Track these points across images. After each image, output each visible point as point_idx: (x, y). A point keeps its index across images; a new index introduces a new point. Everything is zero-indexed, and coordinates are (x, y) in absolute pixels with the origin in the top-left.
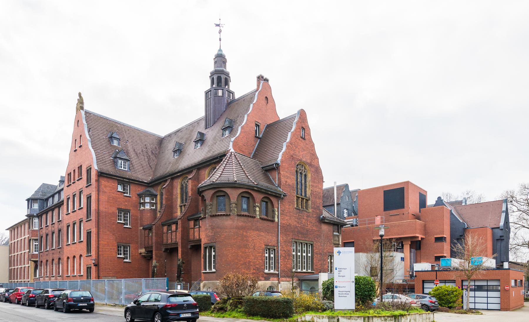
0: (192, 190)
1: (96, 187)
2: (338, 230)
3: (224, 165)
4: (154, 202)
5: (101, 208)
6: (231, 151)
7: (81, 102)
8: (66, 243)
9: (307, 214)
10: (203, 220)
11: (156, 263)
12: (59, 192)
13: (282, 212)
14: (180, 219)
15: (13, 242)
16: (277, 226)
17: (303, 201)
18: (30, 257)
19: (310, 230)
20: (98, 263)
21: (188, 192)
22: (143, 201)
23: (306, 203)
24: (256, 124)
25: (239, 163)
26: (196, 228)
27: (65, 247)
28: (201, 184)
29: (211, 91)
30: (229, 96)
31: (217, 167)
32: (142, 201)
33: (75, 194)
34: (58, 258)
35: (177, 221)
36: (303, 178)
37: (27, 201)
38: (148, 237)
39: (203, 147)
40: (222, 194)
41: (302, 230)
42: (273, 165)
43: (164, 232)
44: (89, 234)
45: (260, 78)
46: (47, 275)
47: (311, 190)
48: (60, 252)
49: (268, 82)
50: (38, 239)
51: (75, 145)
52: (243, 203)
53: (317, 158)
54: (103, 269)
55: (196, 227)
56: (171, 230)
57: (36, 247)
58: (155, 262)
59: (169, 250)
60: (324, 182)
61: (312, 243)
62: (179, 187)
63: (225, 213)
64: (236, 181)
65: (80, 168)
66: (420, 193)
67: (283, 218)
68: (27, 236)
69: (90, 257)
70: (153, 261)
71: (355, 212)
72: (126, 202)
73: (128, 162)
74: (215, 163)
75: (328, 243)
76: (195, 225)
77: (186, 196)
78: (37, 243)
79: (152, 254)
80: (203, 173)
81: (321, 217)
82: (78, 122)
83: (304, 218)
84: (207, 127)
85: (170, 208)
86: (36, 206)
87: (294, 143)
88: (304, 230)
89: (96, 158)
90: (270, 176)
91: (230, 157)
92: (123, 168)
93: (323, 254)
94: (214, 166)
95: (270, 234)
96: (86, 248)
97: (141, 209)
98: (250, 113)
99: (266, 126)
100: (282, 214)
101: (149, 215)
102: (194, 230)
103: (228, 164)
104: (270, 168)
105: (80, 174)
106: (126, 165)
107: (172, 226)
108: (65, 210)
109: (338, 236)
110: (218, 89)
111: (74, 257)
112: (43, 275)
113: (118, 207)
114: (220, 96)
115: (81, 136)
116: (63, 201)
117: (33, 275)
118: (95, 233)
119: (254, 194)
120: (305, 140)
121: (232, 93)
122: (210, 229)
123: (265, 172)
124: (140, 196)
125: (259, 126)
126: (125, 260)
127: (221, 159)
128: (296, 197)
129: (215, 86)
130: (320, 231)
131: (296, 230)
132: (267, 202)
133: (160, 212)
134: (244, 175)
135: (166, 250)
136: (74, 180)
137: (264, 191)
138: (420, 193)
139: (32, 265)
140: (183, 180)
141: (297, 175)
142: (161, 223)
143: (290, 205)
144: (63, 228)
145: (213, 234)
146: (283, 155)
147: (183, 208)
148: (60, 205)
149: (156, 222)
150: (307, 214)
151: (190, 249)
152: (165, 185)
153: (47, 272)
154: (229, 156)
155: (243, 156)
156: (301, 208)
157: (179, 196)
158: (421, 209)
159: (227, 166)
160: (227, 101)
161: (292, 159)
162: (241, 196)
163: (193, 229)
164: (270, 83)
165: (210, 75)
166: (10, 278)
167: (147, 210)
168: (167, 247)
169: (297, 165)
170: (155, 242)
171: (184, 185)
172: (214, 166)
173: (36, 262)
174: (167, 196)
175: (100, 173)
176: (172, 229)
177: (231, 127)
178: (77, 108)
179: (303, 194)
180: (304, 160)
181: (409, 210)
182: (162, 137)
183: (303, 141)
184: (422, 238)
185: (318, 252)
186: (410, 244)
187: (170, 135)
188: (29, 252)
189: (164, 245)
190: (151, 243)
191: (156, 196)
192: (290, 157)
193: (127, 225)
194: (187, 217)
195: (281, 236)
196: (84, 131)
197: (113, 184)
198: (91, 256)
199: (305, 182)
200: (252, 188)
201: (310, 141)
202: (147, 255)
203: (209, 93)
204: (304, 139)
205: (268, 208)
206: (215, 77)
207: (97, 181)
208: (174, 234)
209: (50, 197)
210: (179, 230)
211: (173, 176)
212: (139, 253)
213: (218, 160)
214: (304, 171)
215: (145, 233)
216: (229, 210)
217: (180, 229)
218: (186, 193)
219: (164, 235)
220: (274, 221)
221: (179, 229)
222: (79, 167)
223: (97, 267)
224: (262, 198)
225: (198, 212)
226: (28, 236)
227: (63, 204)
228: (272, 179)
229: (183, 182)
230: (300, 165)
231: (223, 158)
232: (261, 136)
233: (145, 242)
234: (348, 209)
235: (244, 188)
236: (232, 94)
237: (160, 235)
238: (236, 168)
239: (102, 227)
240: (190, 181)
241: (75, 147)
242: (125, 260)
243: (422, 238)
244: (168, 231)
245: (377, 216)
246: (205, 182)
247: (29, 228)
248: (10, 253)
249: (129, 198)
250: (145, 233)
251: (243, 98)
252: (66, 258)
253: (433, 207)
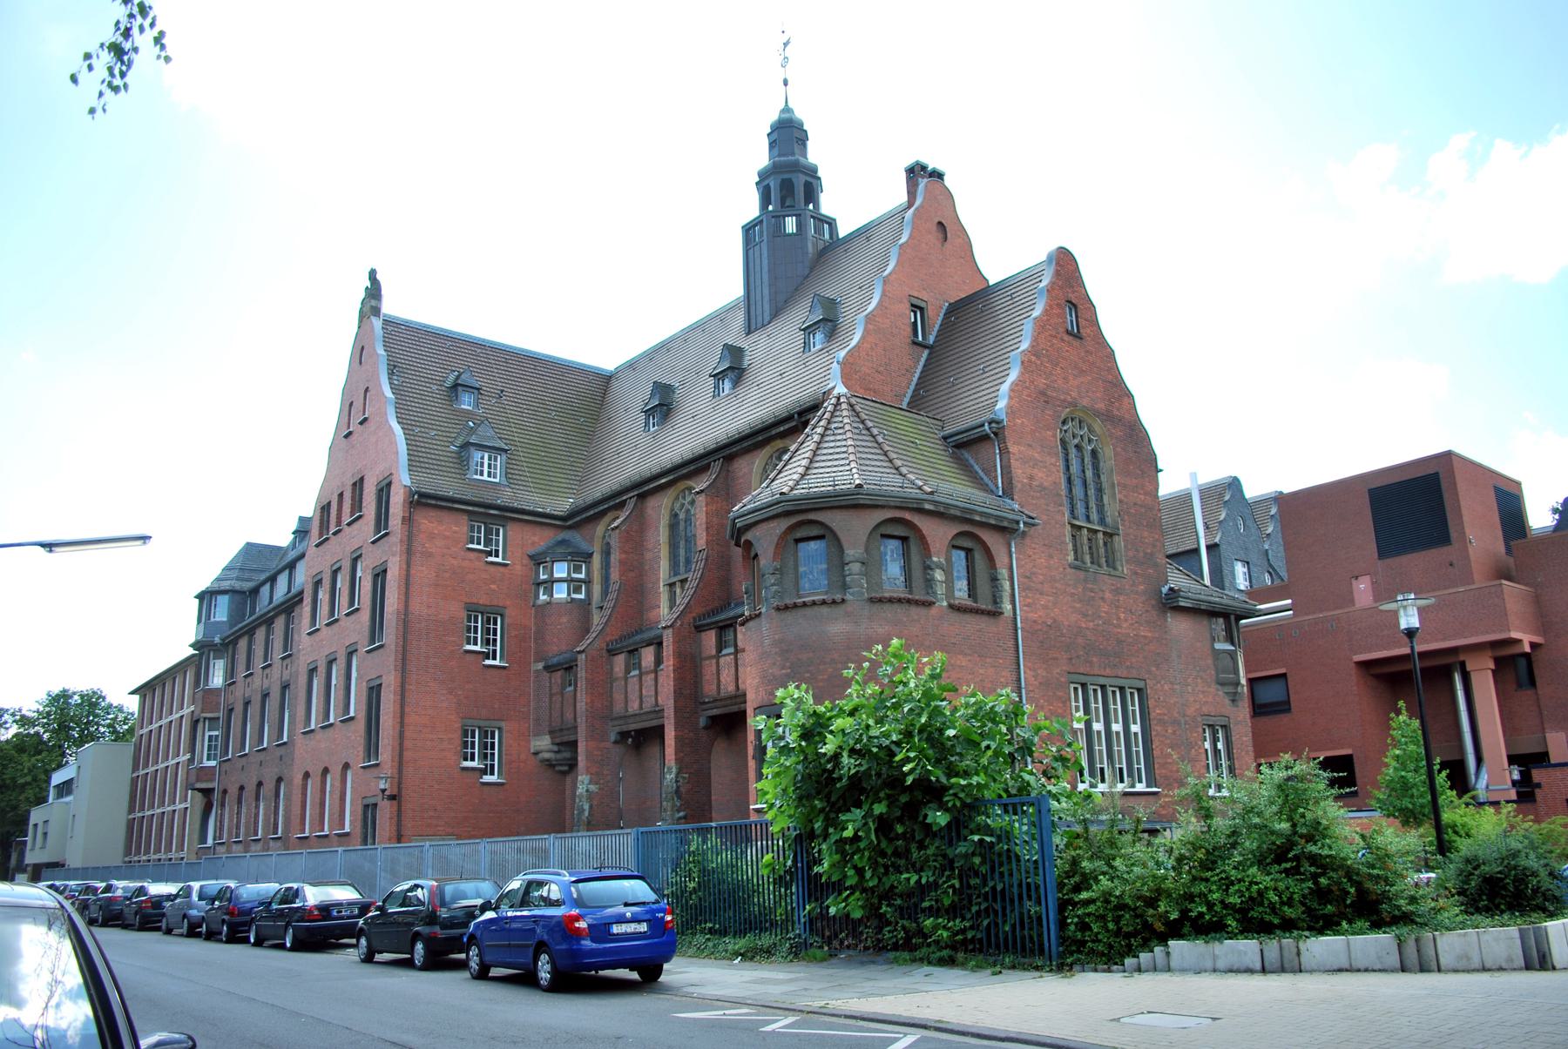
0: (707, 528)
1: (401, 541)
2: (1229, 630)
3: (816, 438)
4: (582, 576)
5: (417, 607)
6: (835, 392)
7: (374, 291)
8: (302, 725)
9: (1113, 585)
10: (751, 624)
11: (590, 783)
12: (291, 566)
13: (1026, 580)
14: (671, 626)
15: (145, 731)
16: (1010, 631)
17: (1097, 539)
18: (193, 778)
19: (1131, 640)
20: (399, 788)
21: (695, 536)
22: (545, 577)
23: (1105, 544)
24: (912, 305)
25: (868, 429)
26: (725, 655)
27: (299, 739)
28: (741, 504)
29: (761, 222)
30: (819, 231)
31: (793, 448)
32: (543, 577)
33: (340, 568)
34: (276, 777)
35: (661, 636)
36: (1086, 462)
37: (197, 600)
38: (562, 695)
39: (741, 390)
40: (815, 532)
41: (1101, 639)
42: (983, 425)
43: (615, 676)
44: (374, 692)
45: (916, 172)
46: (237, 836)
47: (1121, 501)
48: (281, 757)
49: (943, 180)
50: (218, 718)
51: (349, 419)
52: (888, 558)
53: (1130, 395)
54: (414, 811)
55: (724, 652)
56: (640, 668)
57: (491, 637)
58: (586, 782)
59: (631, 737)
60: (1161, 471)
61: (1141, 685)
62: (664, 522)
63: (825, 597)
64: (859, 486)
65: (359, 485)
66: (1497, 489)
67: (1030, 601)
68: (186, 711)
69: (375, 771)
70: (579, 778)
71: (1274, 569)
72: (494, 583)
73: (504, 457)
74: (783, 435)
75: (1199, 681)
76: (720, 647)
77: (688, 550)
78: (215, 733)
79: (576, 752)
80: (745, 470)
81: (1165, 590)
82: (360, 352)
83: (1102, 598)
84: (753, 327)
85: (635, 593)
86: (221, 612)
87: (1047, 351)
88: (1108, 640)
89: (406, 452)
90: (972, 461)
91: (835, 410)
92: (485, 477)
93: (1183, 722)
94: (781, 446)
95: (988, 660)
96: (362, 741)
97: (539, 602)
98: (890, 274)
99: (945, 308)
100: (1023, 589)
101: (564, 620)
102: (718, 663)
103: (829, 432)
104: (972, 437)
105: (357, 504)
106: (496, 466)
107: (643, 655)
108: (306, 620)
109: (1232, 656)
110: (784, 217)
111: (326, 771)
112: (225, 836)
113: (468, 601)
114: (790, 235)
115: (367, 390)
116: (301, 592)
117: (196, 836)
118: (392, 688)
119: (925, 525)
120: (1081, 338)
121: (827, 223)
122: (776, 653)
123: (955, 450)
124: (538, 560)
125: (921, 309)
126: (487, 778)
127: (803, 419)
128: (1068, 527)
129: (775, 206)
130: (1164, 642)
131: (1080, 640)
132: (968, 551)
133: (601, 608)
134: (885, 464)
135: (624, 735)
136: (339, 522)
137: (958, 514)
138: (1497, 489)
139: (193, 801)
140: (677, 498)
141: (1067, 455)
142: (604, 646)
143: (1051, 557)
144: (297, 677)
145: (789, 671)
146: (1012, 390)
147: (678, 591)
148: (290, 606)
149: (588, 642)
150: (1113, 585)
151: (706, 728)
152: (618, 518)
153: (238, 828)
154: (830, 408)
155: (877, 405)
156: (1092, 563)
157: (664, 553)
158: (1512, 543)
159: (827, 439)
160: (815, 245)
161: (1045, 402)
162: (882, 532)
163: (714, 661)
164: (948, 181)
165: (758, 179)
166: (128, 852)
167: (560, 604)
168: (625, 728)
169: (1064, 422)
170: (584, 709)
171: (682, 516)
172: (779, 444)
173: (207, 793)
174: (624, 556)
176: (643, 664)
177: (831, 321)
178: (361, 311)
179: (1094, 516)
180: (1085, 402)
181: (1470, 550)
182: (607, 371)
183: (1076, 343)
184: (1533, 645)
185: (1166, 717)
186: (1493, 667)
187: (631, 366)
188: (191, 761)
189: (616, 719)
190: (572, 716)
192: (1033, 395)
193: (494, 658)
194: (694, 619)
195: (1029, 664)
196: (378, 374)
198: (377, 765)
199: (1094, 474)
200: (915, 506)
201: (1098, 343)
202: (559, 756)
203: (754, 231)
204: (1078, 336)
205: (974, 572)
206: (773, 184)
207: (408, 520)
208: (649, 680)
209: (263, 583)
210: (665, 664)
211: (645, 489)
212: (532, 751)
213: (794, 424)
214: (1090, 441)
215: (553, 681)
216: (840, 584)
217: (671, 663)
218: (686, 541)
220: (1002, 613)
221: (668, 660)
222: (354, 484)
223: (395, 802)
224: (953, 538)
225: (727, 601)
226: (192, 708)
227: (301, 600)
228: (980, 471)
229: (677, 506)
230: (1072, 420)
231: (812, 416)
232: (931, 339)
233: (551, 714)
234: (1248, 563)
235: (890, 507)
236: (830, 224)
237: (603, 686)
238: (859, 443)
239: (414, 669)
240: (701, 499)
241: (349, 424)
242: (487, 778)
243: (1533, 645)
244: (628, 671)
245: (1357, 578)
246: (755, 497)
247: (197, 683)
248: (135, 768)
249: (501, 569)
251: (864, 233)
252: (301, 777)
253: (1554, 535)
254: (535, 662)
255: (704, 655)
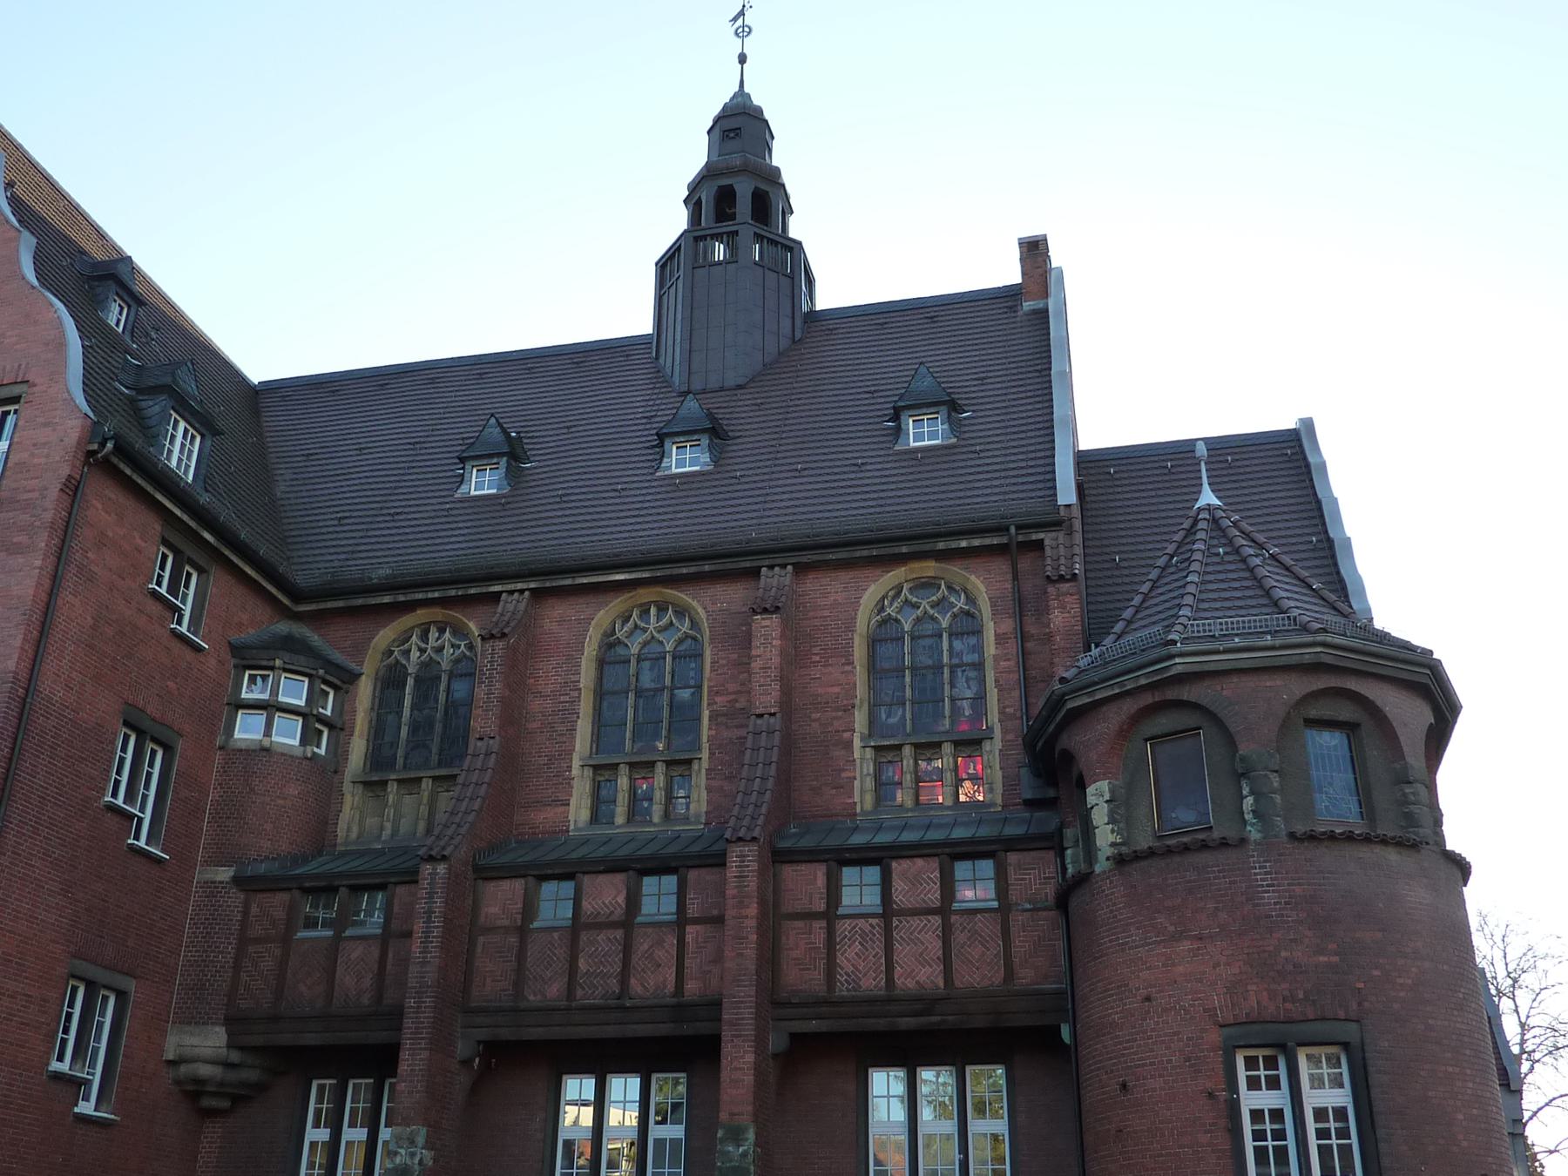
5: (51, 686)
40: (1346, 712)
101: (293, 790)
124: (248, 657)
167: (285, 756)
175: (110, 445)
191: (344, 680)
197: (139, 541)
202: (232, 1076)
206: (706, 196)
213: (1005, 540)
219: (481, 939)
250: (246, 913)
254: (206, 863)
255: (786, 908)
